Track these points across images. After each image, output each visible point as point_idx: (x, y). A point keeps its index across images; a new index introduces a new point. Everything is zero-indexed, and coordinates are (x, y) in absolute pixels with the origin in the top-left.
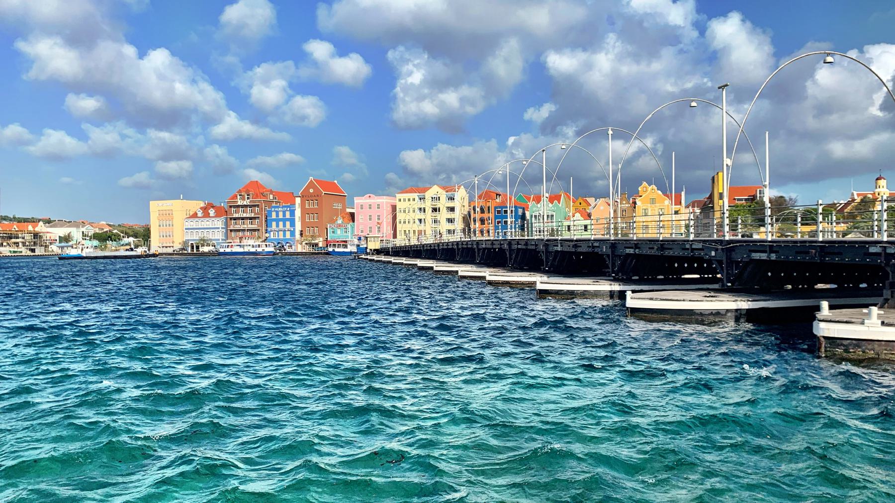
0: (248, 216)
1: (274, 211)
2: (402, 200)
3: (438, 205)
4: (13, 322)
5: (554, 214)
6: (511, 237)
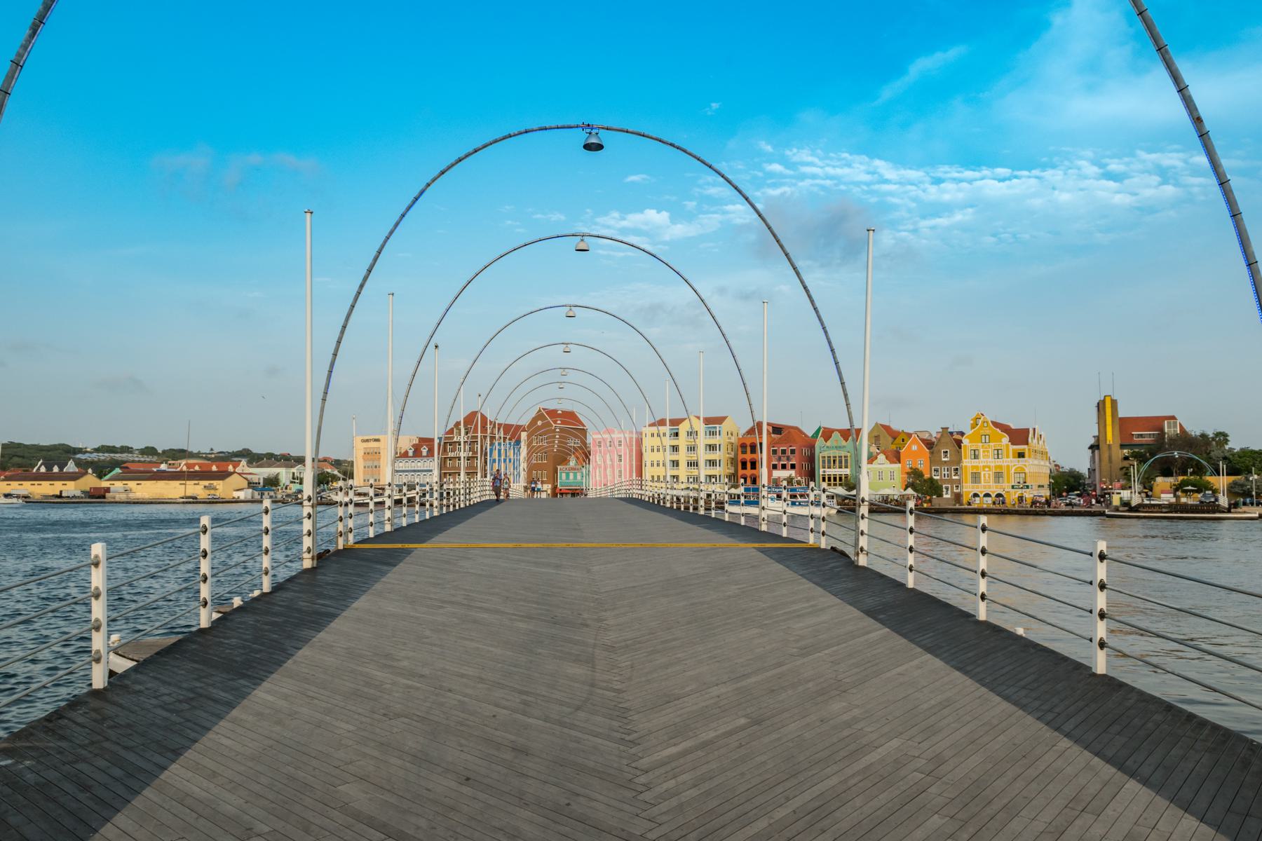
5: (849, 455)
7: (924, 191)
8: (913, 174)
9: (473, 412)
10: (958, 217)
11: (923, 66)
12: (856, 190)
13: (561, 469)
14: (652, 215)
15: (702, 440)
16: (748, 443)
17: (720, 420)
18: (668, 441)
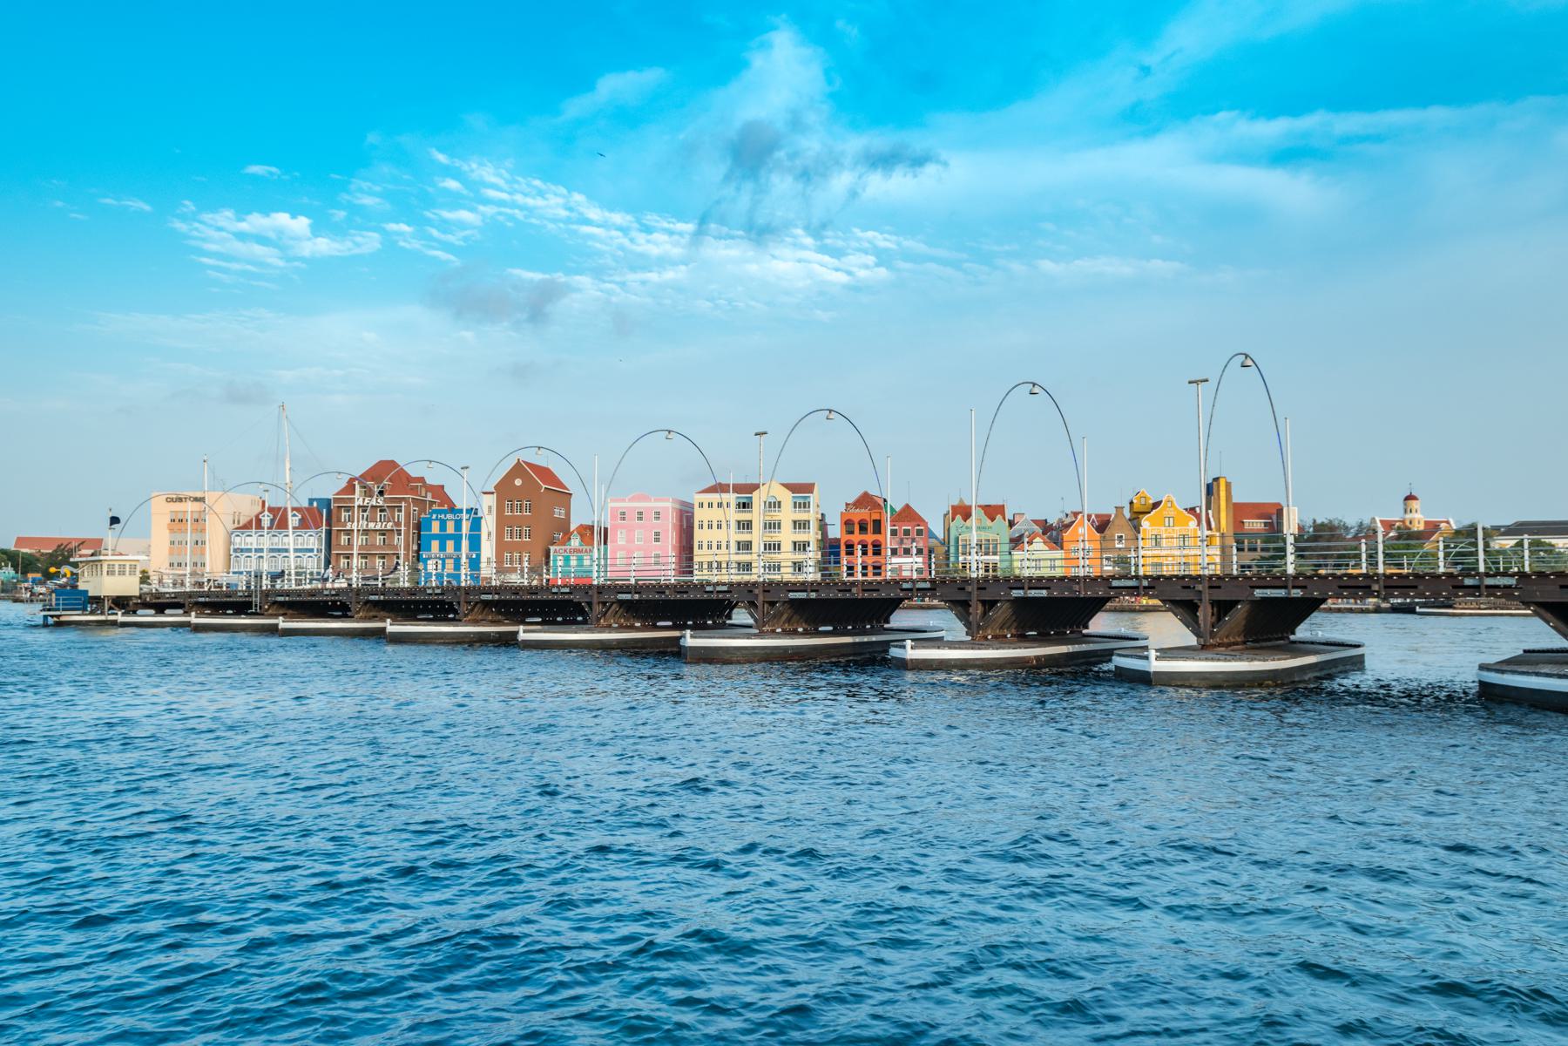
0: (378, 527)
1: (437, 519)
2: (706, 505)
3: (776, 516)
4: (75, 989)
6: (864, 575)
7: (632, 240)
8: (618, 218)
9: (393, 462)
10: (669, 275)
11: (616, 86)
12: (551, 226)
13: (555, 551)
14: (282, 219)
15: (787, 515)
16: (856, 520)
17: (808, 488)
18: (734, 515)
